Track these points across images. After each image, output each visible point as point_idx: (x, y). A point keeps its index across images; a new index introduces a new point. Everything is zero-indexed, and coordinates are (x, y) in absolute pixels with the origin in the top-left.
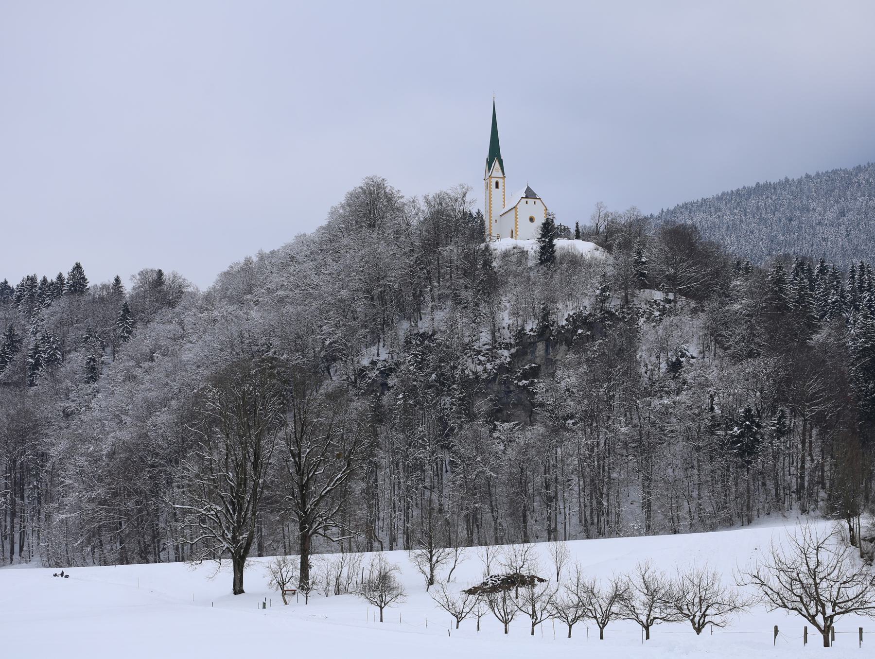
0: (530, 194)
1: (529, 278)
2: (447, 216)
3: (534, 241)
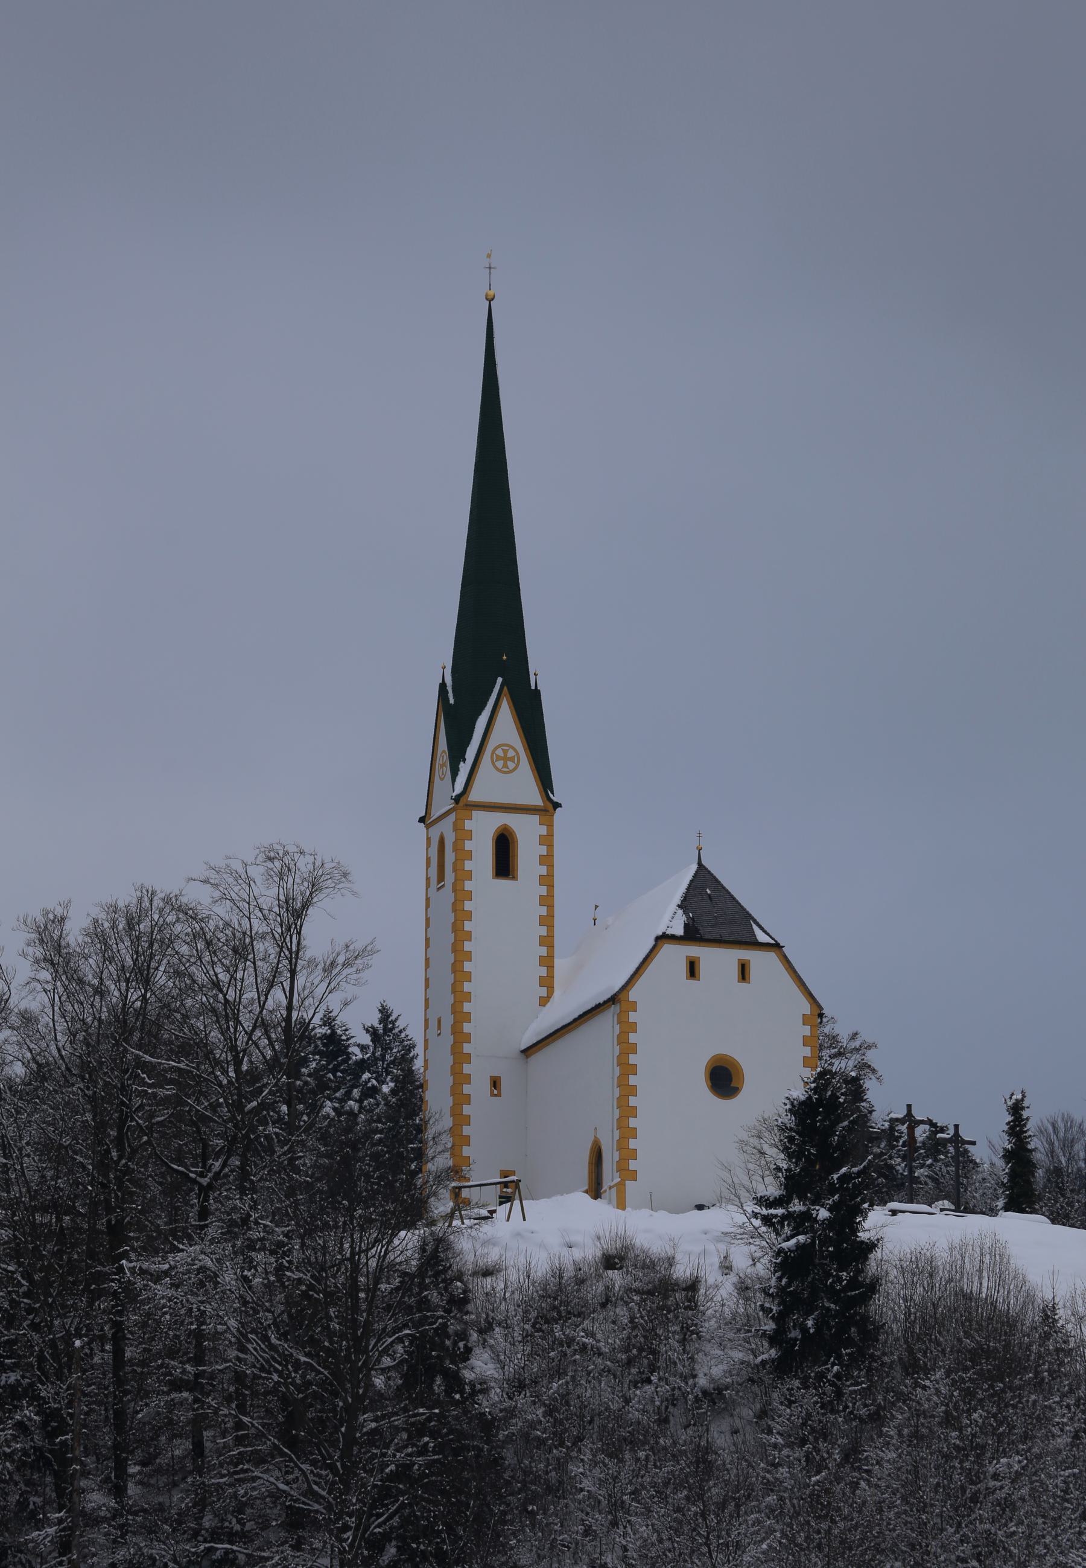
0: (713, 917)
1: (704, 1461)
2: (184, 1049)
3: (727, 1218)
